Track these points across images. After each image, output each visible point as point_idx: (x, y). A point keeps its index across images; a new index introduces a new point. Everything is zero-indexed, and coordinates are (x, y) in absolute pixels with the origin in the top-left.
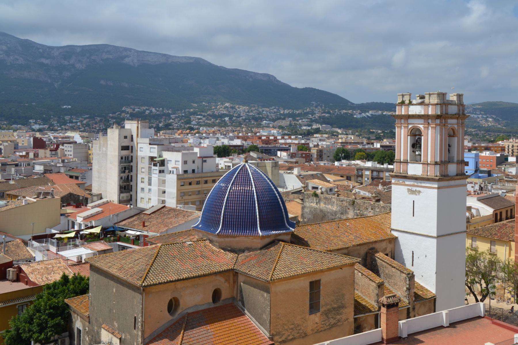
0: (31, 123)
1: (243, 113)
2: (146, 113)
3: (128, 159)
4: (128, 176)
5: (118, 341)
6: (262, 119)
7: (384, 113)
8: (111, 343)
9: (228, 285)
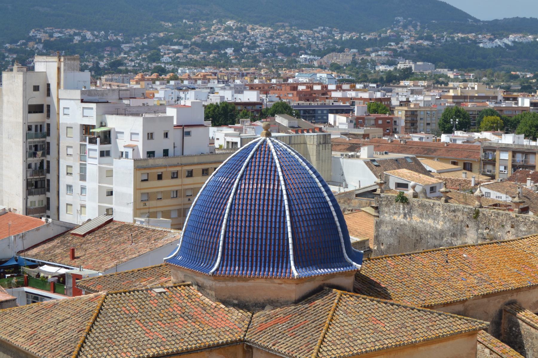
2: (75, 42)
4: (42, 163)
6: (298, 51)
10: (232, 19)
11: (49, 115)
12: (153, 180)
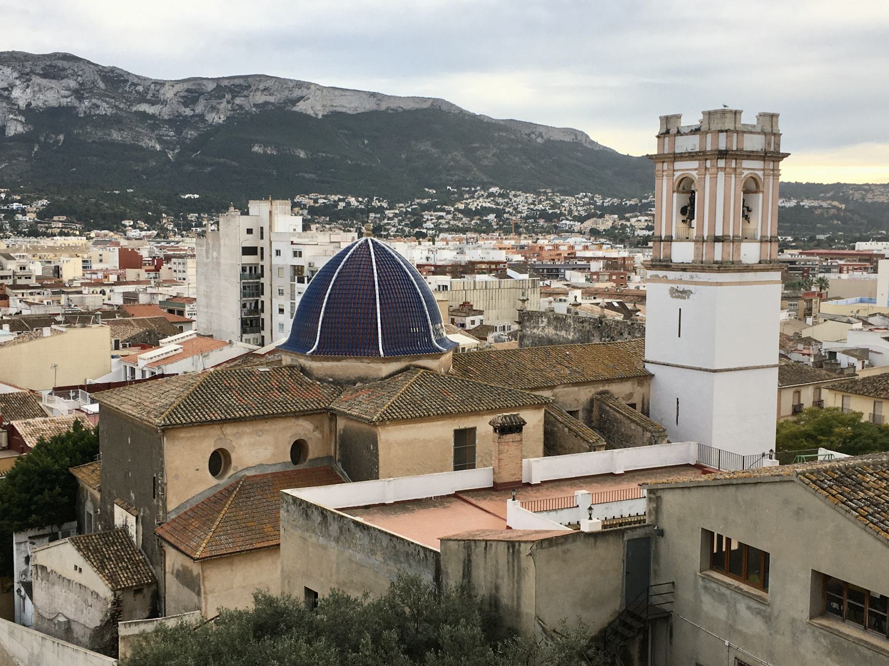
0: (125, 226)
1: (524, 206)
2: (340, 207)
3: (255, 272)
4: (257, 302)
5: (134, 518)
6: (558, 217)
7: (802, 204)
8: (126, 525)
9: (320, 436)
10: (495, 185)
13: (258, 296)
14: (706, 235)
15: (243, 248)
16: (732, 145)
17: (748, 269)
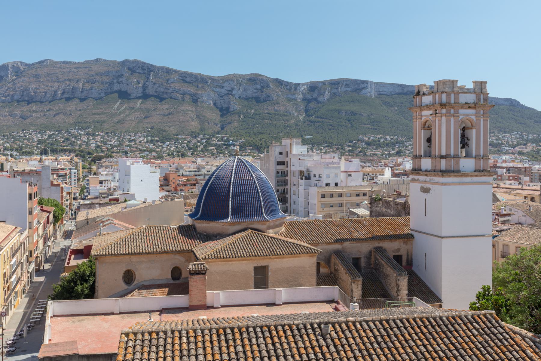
3: (284, 173)
4: (284, 189)
11: (280, 165)
12: (328, 197)
13: (285, 185)
14: (437, 154)
15: (277, 162)
16: (450, 100)
17: (465, 174)
